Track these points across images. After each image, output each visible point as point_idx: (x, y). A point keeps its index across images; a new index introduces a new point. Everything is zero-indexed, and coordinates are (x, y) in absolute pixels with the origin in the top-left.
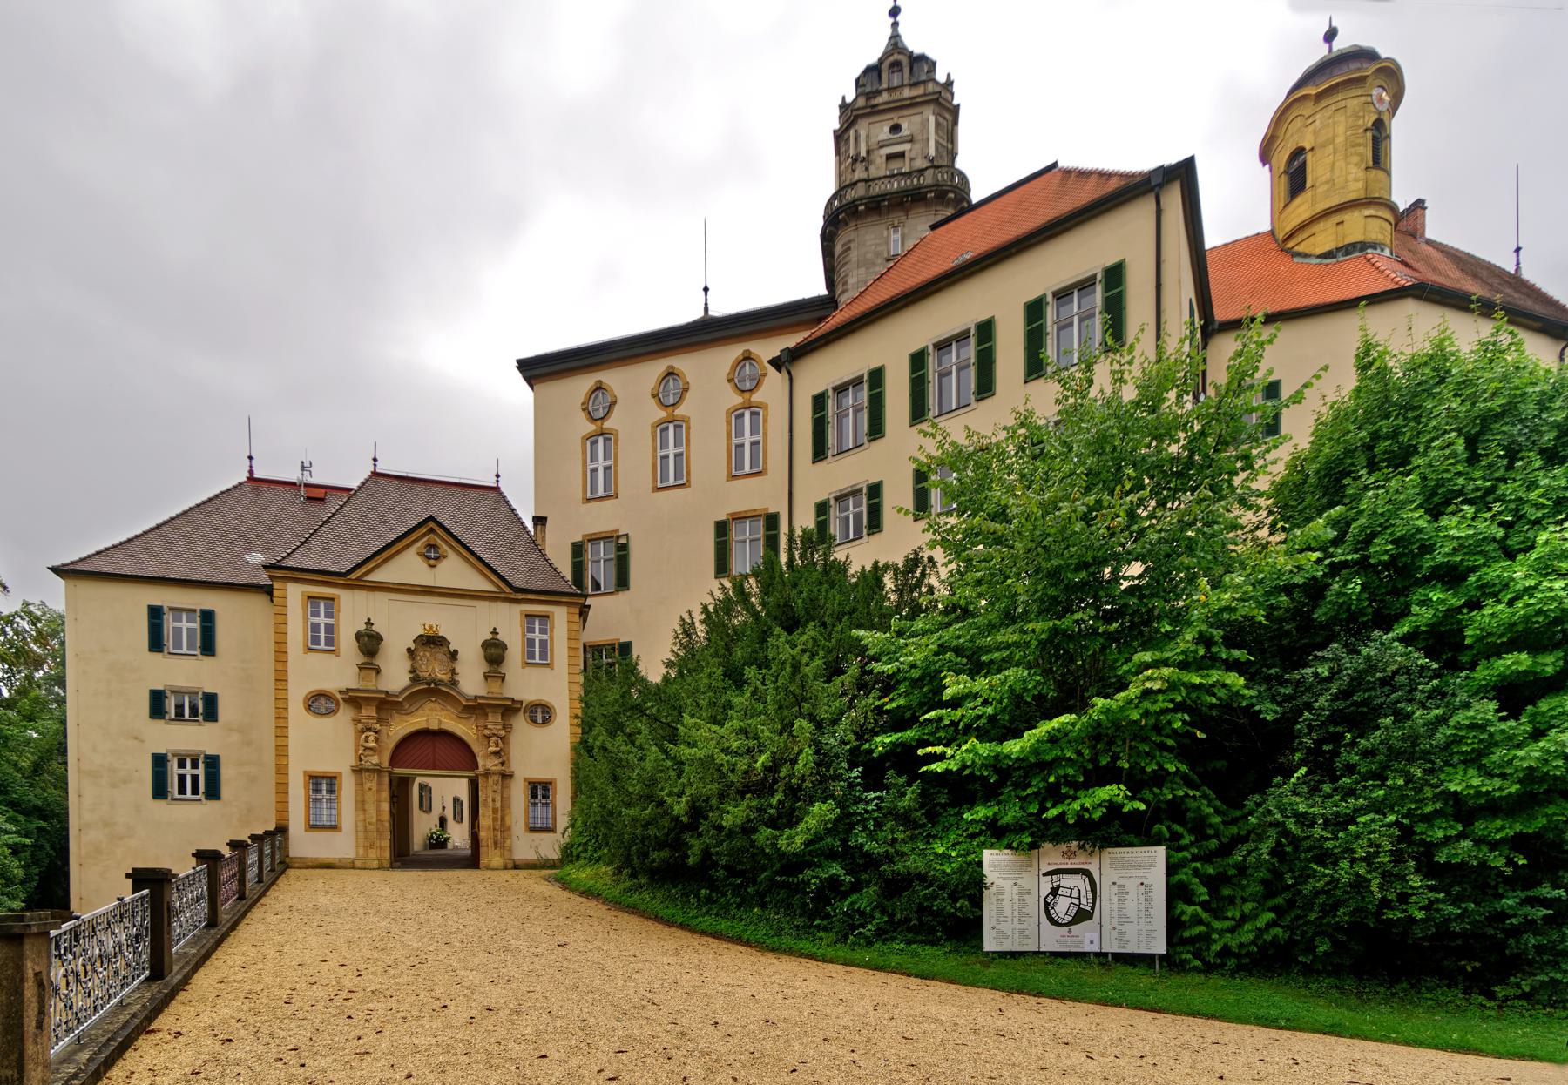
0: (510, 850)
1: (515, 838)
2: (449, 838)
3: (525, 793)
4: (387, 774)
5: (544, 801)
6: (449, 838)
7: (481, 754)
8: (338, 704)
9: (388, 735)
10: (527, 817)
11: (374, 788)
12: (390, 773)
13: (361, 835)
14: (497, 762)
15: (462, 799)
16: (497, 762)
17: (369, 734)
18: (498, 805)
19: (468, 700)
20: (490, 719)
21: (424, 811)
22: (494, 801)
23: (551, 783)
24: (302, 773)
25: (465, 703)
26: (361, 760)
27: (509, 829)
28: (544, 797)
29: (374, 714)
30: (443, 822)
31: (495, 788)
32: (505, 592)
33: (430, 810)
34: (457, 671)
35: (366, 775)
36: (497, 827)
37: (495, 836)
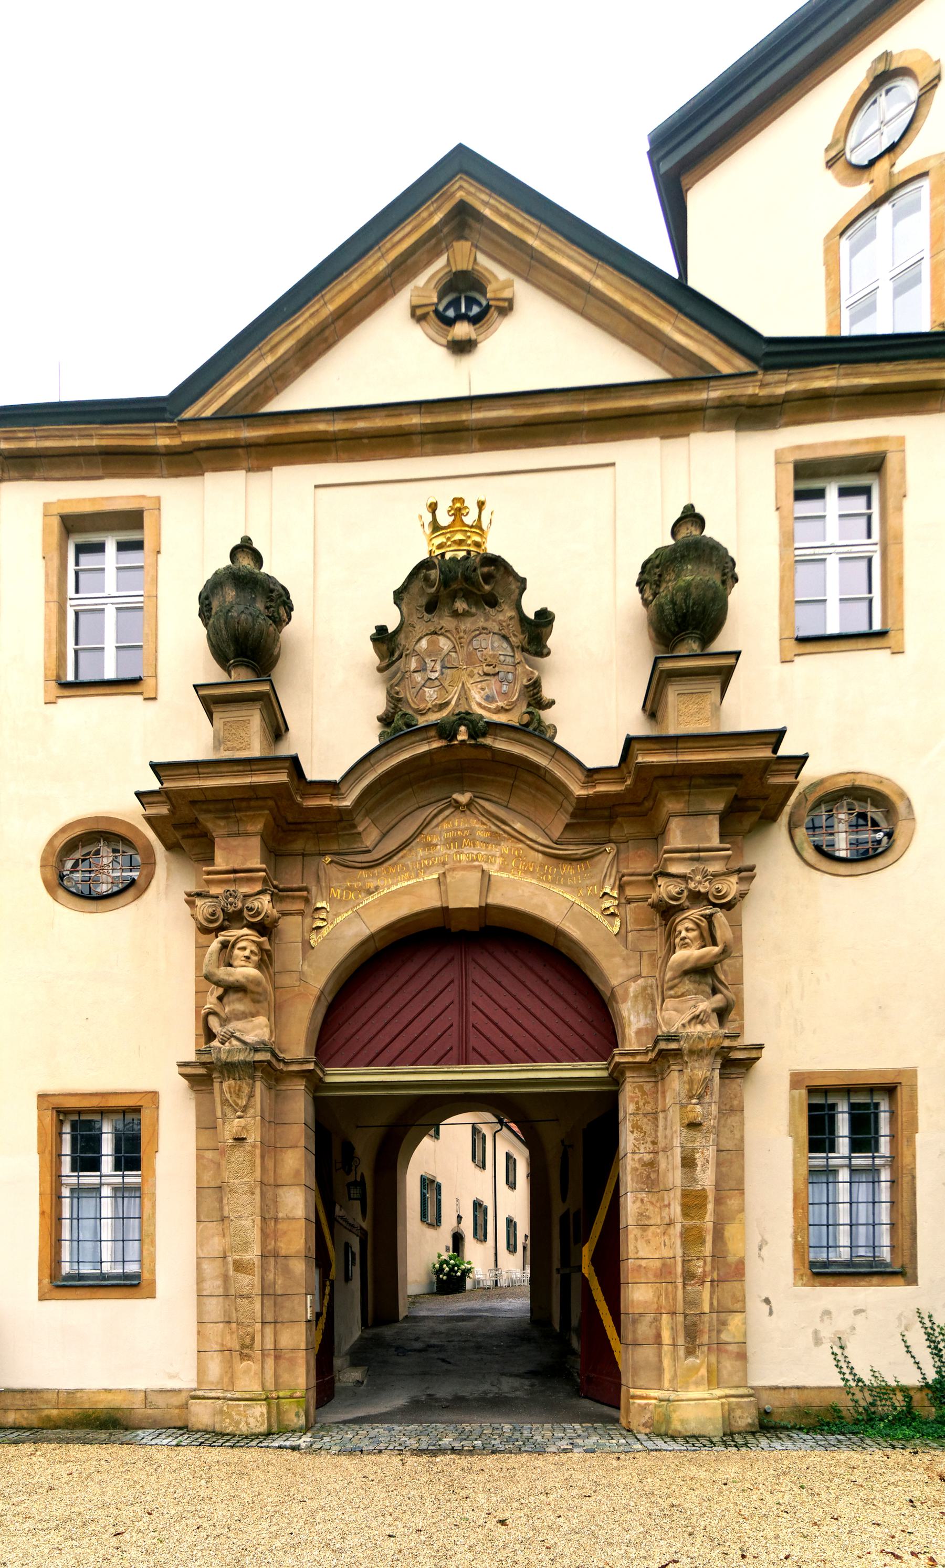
0: (742, 1356)
1: (755, 1307)
2: (469, 1271)
3: (793, 1132)
5: (861, 1160)
7: (633, 988)
8: (150, 862)
9: (307, 946)
10: (802, 1224)
11: (254, 1137)
12: (315, 1084)
13: (214, 1307)
17: (232, 934)
18: (706, 1178)
19: (592, 774)
20: (676, 837)
22: (688, 1163)
23: (890, 1090)
24: (34, 1102)
25: (578, 791)
26: (210, 1035)
27: (738, 1271)
28: (856, 1146)
29: (256, 863)
30: (458, 1239)
32: (713, 377)
33: (437, 1222)
34: (547, 693)
35: (224, 1087)
36: (698, 1268)
37: (691, 1302)
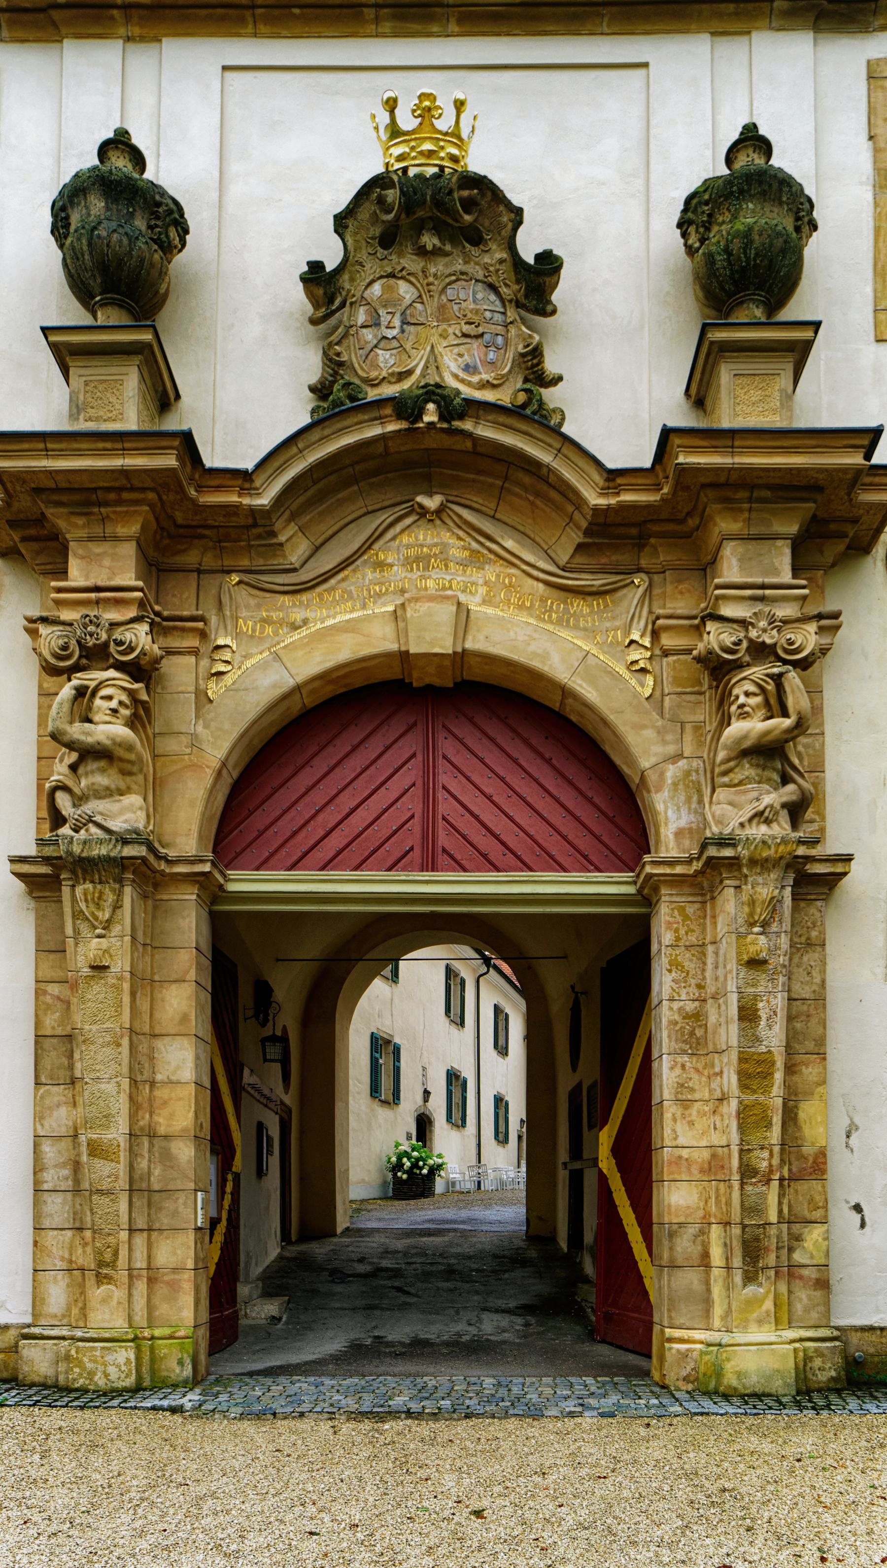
0: (823, 1284)
2: (440, 1167)
4: (189, 895)
6: (440, 1167)
7: (671, 772)
9: (202, 699)
11: (120, 965)
14: (771, 798)
15: (494, 1053)
16: (771, 798)
21: (385, 1103)
25: (594, 499)
26: (57, 819)
29: (128, 578)
30: (424, 1124)
31: (760, 944)
34: (551, 365)
37: (751, 1209)
